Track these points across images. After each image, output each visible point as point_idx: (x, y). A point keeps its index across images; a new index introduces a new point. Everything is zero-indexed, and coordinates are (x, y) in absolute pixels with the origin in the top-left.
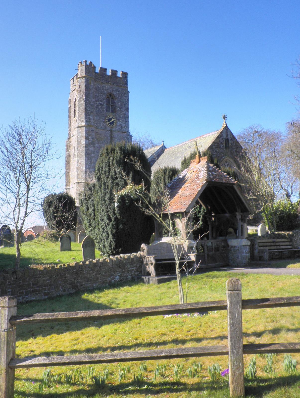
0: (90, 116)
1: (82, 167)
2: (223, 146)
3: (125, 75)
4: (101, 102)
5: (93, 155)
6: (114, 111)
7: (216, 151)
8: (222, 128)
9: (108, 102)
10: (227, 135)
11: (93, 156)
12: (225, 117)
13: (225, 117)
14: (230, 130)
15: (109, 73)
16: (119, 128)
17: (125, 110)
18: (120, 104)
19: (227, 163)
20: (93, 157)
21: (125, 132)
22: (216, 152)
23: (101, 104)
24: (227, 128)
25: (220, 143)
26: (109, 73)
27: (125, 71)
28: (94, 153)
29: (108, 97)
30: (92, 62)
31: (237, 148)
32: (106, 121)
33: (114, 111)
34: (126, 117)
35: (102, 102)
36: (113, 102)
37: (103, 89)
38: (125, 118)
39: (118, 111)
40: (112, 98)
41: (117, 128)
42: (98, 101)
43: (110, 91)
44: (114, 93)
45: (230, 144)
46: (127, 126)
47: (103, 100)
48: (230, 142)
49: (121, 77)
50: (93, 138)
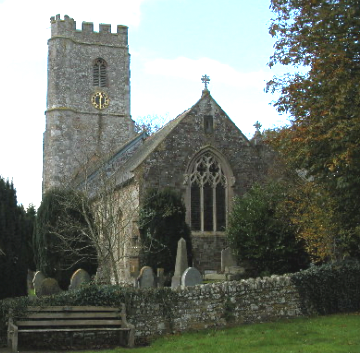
0: (64, 94)
1: (51, 171)
2: (201, 128)
3: (123, 29)
4: (84, 74)
5: (68, 152)
6: (105, 84)
7: (186, 138)
8: (199, 96)
9: (96, 71)
10: (209, 110)
11: (68, 153)
12: (206, 79)
13: (206, 79)
14: (214, 101)
15: (97, 29)
16: (113, 111)
17: (123, 81)
18: (114, 73)
19: (210, 158)
20: (68, 155)
21: (122, 116)
22: (187, 140)
23: (83, 76)
24: (206, 94)
25: (193, 124)
26: (97, 29)
27: (124, 24)
28: (69, 149)
29: (96, 65)
30: (69, 15)
31: (229, 130)
32: (92, 100)
33: (105, 84)
34: (126, 94)
35: (85, 72)
36: (104, 72)
37: (87, 53)
38: (123, 94)
39: (113, 84)
40: (103, 65)
41: (110, 109)
42: (80, 71)
43: (100, 55)
44: (105, 58)
45: (214, 126)
46: (128, 107)
47: (88, 69)
48: (214, 121)
49: (81, 29)
50: (68, 127)
